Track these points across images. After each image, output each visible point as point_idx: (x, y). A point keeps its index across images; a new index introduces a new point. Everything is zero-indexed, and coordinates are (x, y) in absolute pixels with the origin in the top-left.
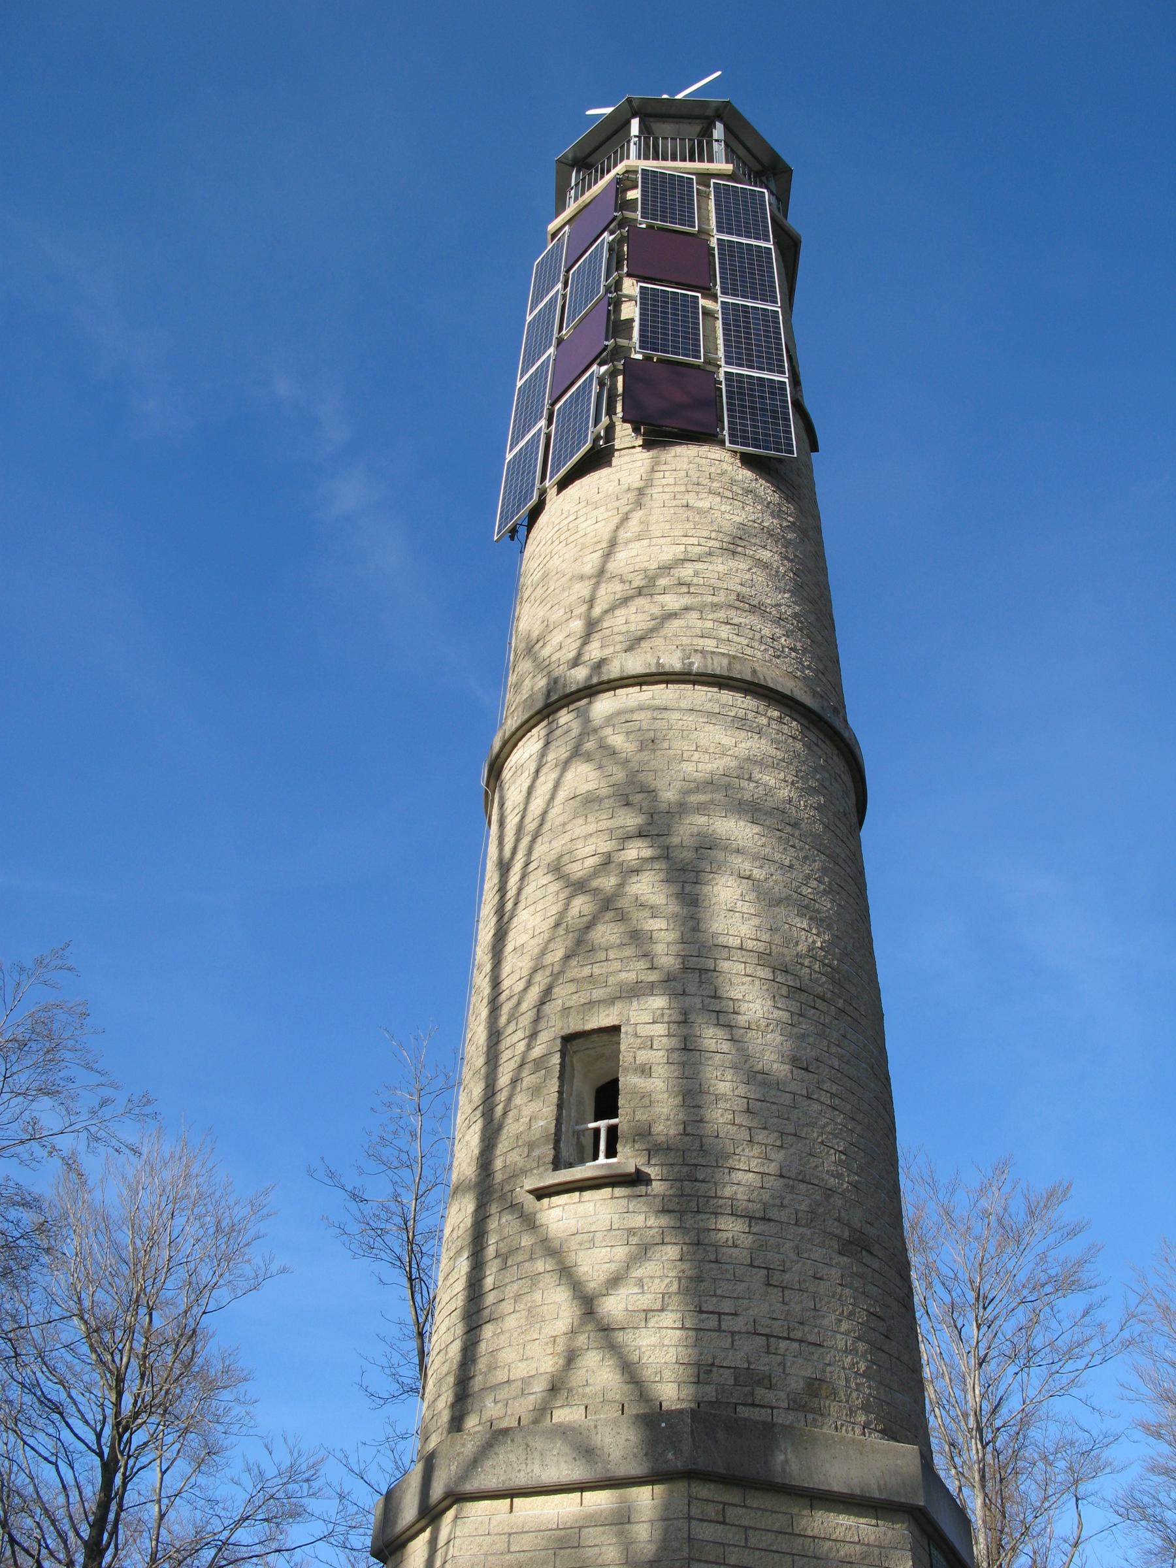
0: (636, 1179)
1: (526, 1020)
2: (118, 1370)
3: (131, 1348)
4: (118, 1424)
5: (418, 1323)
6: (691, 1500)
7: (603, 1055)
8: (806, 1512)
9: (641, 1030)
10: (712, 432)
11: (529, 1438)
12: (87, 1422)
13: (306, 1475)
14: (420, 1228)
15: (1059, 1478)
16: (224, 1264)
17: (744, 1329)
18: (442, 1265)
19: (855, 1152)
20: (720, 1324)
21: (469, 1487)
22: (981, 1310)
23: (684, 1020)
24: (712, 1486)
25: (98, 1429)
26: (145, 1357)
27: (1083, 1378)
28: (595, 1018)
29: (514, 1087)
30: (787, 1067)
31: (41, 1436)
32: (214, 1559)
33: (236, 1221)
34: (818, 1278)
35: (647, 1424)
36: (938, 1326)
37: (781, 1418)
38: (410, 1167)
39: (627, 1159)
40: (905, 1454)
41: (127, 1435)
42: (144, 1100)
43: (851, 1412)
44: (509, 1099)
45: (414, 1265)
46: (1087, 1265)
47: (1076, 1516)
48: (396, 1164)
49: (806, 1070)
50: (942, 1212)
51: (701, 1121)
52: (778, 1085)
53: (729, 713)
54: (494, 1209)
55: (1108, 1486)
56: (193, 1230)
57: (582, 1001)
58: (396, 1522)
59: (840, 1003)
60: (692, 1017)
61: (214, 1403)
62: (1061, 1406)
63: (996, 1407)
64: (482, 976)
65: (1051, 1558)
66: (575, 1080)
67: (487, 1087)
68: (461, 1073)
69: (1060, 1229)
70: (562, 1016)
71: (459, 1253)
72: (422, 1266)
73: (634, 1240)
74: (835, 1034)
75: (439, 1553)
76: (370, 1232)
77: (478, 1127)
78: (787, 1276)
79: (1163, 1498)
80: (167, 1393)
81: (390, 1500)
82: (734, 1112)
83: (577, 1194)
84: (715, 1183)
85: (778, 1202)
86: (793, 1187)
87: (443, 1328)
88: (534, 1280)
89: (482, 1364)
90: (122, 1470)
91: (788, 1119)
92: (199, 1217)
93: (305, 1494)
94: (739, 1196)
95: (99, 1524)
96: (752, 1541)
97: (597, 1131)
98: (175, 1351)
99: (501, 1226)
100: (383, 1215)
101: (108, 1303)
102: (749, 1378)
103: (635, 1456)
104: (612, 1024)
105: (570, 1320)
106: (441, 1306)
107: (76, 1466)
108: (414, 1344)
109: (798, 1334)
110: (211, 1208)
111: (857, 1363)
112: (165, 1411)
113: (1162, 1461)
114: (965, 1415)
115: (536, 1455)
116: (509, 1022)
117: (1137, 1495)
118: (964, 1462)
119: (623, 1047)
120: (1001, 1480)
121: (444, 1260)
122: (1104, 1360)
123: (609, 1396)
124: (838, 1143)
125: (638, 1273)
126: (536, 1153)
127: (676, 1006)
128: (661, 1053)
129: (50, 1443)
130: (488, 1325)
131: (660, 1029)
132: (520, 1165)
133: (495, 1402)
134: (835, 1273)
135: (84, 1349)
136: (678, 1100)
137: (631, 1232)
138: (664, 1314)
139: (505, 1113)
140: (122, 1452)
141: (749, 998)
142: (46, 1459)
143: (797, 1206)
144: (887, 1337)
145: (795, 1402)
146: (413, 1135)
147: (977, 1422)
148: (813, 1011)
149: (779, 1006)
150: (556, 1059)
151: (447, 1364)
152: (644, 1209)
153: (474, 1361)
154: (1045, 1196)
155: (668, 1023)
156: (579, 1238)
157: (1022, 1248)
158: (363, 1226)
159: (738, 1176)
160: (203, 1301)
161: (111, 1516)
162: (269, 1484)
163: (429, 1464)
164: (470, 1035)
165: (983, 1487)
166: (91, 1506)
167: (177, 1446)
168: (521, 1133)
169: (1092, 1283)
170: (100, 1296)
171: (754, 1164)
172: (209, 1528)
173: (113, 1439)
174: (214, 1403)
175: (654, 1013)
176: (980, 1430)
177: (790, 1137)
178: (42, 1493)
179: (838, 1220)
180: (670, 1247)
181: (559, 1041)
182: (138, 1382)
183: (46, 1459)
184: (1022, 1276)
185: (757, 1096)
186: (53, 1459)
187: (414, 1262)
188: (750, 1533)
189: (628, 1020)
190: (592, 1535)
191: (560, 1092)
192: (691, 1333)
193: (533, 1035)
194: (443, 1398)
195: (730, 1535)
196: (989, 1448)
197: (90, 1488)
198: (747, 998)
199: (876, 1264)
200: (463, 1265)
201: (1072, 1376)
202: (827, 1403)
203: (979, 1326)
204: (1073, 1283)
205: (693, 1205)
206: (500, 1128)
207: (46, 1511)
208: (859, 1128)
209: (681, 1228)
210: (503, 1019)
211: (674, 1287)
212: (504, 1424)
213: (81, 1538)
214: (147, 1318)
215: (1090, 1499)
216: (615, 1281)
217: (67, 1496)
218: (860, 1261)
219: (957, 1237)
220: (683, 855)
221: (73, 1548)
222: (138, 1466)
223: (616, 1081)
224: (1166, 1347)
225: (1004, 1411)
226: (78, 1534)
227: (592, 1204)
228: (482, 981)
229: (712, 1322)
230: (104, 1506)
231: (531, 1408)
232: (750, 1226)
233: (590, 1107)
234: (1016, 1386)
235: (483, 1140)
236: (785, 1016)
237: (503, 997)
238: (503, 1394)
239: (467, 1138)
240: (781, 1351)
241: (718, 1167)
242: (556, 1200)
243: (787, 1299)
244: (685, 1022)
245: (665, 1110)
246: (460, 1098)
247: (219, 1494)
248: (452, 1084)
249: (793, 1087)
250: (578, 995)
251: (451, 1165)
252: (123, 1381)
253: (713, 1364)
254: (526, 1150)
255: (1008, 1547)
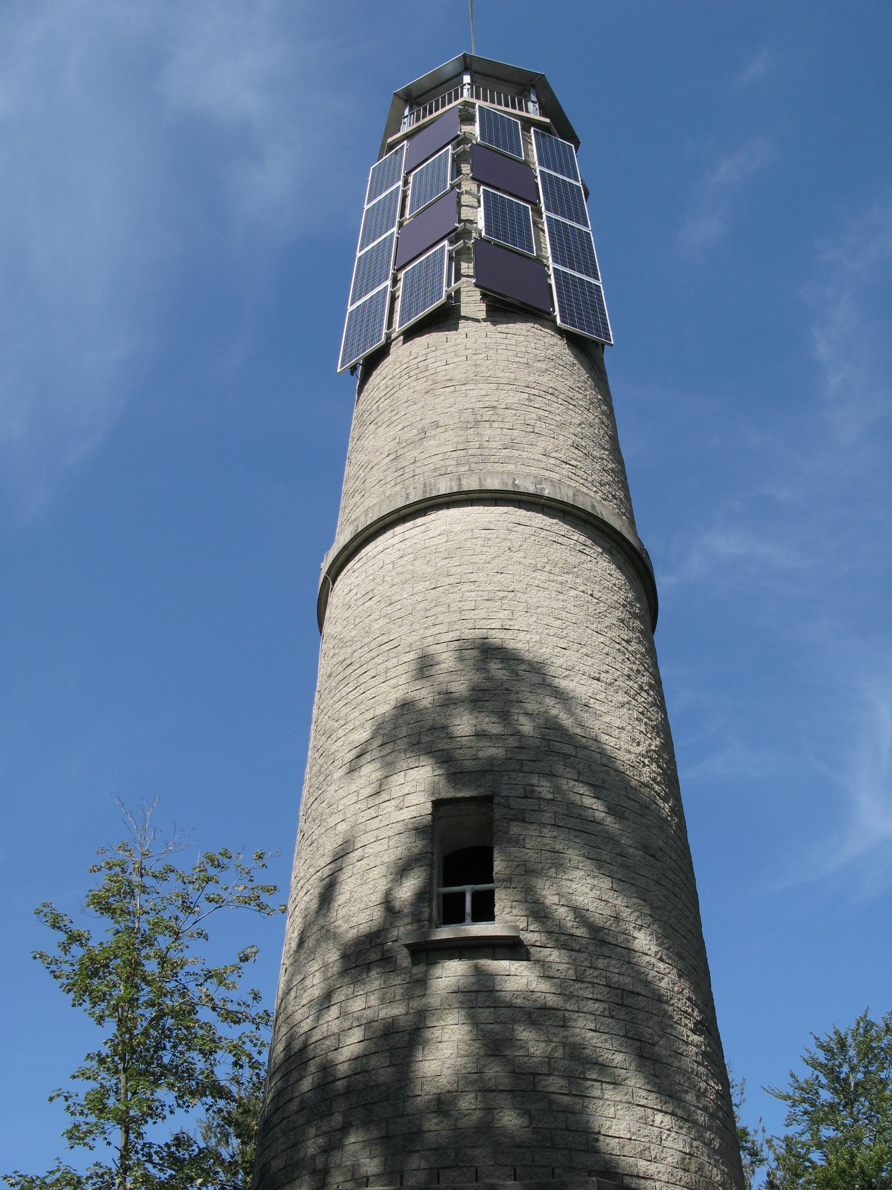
10: (545, 310)
34: (679, 1053)
53: (572, 537)
104: (484, 794)
111: (714, 1139)
220: (542, 651)
240: (657, 1123)
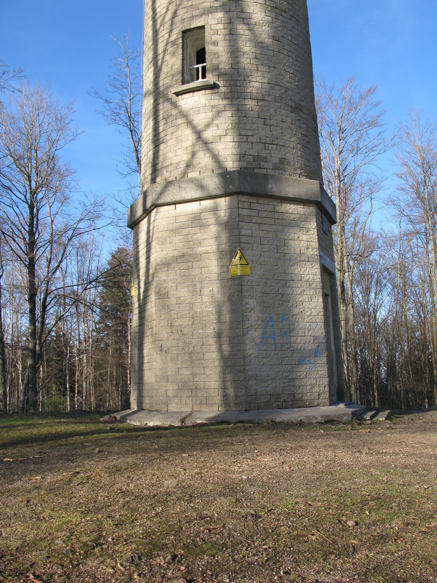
0: (214, 87)
1: (167, 25)
2: (28, 173)
3: (31, 165)
4: (31, 192)
5: (135, 147)
6: (239, 202)
7: (198, 38)
8: (279, 204)
9: (213, 27)
11: (180, 184)
12: (20, 192)
13: (101, 204)
14: (133, 111)
15: (366, 192)
16: (61, 131)
17: (256, 141)
18: (143, 124)
19: (297, 73)
20: (247, 140)
21: (160, 202)
22: (341, 134)
23: (230, 22)
24: (246, 197)
25: (25, 194)
26: (37, 168)
27: (376, 158)
28: (194, 23)
29: (165, 53)
30: (271, 40)
31: (5, 198)
32: (73, 233)
33: (63, 115)
35: (222, 177)
36: (325, 140)
37: (270, 172)
38: (126, 88)
39: (210, 79)
40: (314, 184)
41: (35, 195)
42: (20, 71)
43: (295, 170)
44: (163, 58)
45: (132, 125)
46: (381, 117)
47: (371, 205)
48: (121, 88)
49: (278, 41)
50: (328, 97)
51: (238, 63)
52: (267, 48)
54: (161, 101)
55: (382, 194)
56: (47, 119)
57: (189, 16)
58: (135, 215)
59: (292, 13)
60: (233, 21)
61: (65, 182)
62: (368, 168)
63: (345, 168)
64: (148, 8)
65: (361, 218)
66: (188, 49)
67: (154, 53)
68: (143, 48)
69: (372, 104)
70: (181, 23)
71: (149, 119)
72: (135, 125)
73: (214, 110)
74: (289, 26)
75: (151, 224)
76: (114, 114)
77: (152, 69)
78: (271, 121)
79: (401, 198)
80: (47, 180)
81: (132, 208)
82: (250, 59)
83: (192, 93)
84: (244, 87)
85: (268, 93)
86: (273, 87)
87: (145, 147)
88: (178, 126)
89: (161, 159)
90: (36, 207)
91: (271, 61)
92: (48, 115)
93: (101, 210)
94: (253, 92)
95: (31, 225)
96: (261, 214)
97: (198, 69)
98: (47, 165)
99: (164, 107)
100: (118, 107)
101: (20, 150)
102: (258, 159)
103: (218, 187)
105: (192, 141)
106: (144, 139)
107: (19, 207)
108: (134, 154)
109: (276, 142)
110: (52, 111)
112: (47, 186)
113: (401, 186)
114: (334, 171)
115: (183, 189)
116: (161, 26)
117: (392, 197)
118: (333, 188)
119: (206, 34)
120: (346, 193)
121: (143, 122)
122: (384, 152)
123: (208, 167)
124: (290, 70)
125: (216, 122)
126: (175, 79)
127: (226, 16)
128: (221, 36)
129: (9, 201)
130: (162, 144)
131: (221, 26)
132: (169, 84)
133: (167, 172)
134: (289, 120)
135: (14, 167)
136: (229, 55)
137: (213, 107)
138: (226, 137)
139: (162, 64)
140: (35, 201)
141: (255, 12)
142: (8, 206)
143: (275, 95)
144: (308, 143)
145: (275, 166)
146: (127, 76)
147: (338, 174)
148: (281, 17)
149: (267, 15)
150: (180, 41)
151: (148, 160)
152: (218, 98)
153: (158, 158)
154: (367, 91)
155: (224, 23)
156: (193, 110)
157: (357, 111)
158: (111, 112)
159: (252, 84)
160: (55, 146)
161: (35, 223)
162: (88, 208)
163: (145, 195)
164: (145, 33)
165: (339, 196)
166: (28, 220)
167: (54, 197)
168: (169, 71)
169: (382, 124)
170: (17, 147)
171: (258, 79)
172: (69, 224)
173: (31, 197)
174: (65, 182)
175: (218, 20)
176: (339, 176)
177: (272, 68)
178: (10, 217)
179: (291, 100)
180: (228, 112)
181: (181, 33)
182: (36, 177)
183: (8, 206)
184: (356, 122)
185: (259, 52)
186: (11, 206)
187: (131, 124)
188: (260, 212)
189: (208, 23)
190: (204, 215)
191: (183, 54)
192: (237, 143)
193: (171, 31)
194: (148, 172)
195: (253, 213)
196: (342, 183)
197: (26, 214)
198: (255, 12)
199: (304, 116)
200: (151, 123)
201: (373, 157)
202: (287, 166)
203: (340, 140)
204: (375, 124)
205: (236, 95)
206: (160, 70)
207: (12, 222)
208: (298, 64)
209: (232, 105)
210: (158, 26)
211: (230, 127)
212: (171, 179)
213: (26, 230)
214: (35, 154)
215: (375, 199)
216: (208, 126)
217: (18, 217)
218: (299, 115)
219: (333, 107)
221: (24, 234)
222: (41, 205)
223: (204, 48)
224: (407, 147)
225: (348, 170)
226: (25, 229)
227: (198, 97)
228: (148, 10)
229: (244, 139)
230: (32, 220)
231: (180, 173)
232: (257, 103)
233: (194, 59)
234: (352, 161)
235: (154, 75)
236: (270, 19)
237: (158, 16)
238: (170, 168)
239: (148, 74)
240: (270, 149)
241: (245, 80)
242: (184, 96)
243: (272, 130)
244: (230, 23)
245: (224, 59)
246: (144, 59)
247: (71, 212)
248: (140, 54)
249: (273, 48)
250: (187, 14)
251: (143, 86)
252: (30, 177)
253: (245, 154)
254: (171, 77)
255: (347, 215)
